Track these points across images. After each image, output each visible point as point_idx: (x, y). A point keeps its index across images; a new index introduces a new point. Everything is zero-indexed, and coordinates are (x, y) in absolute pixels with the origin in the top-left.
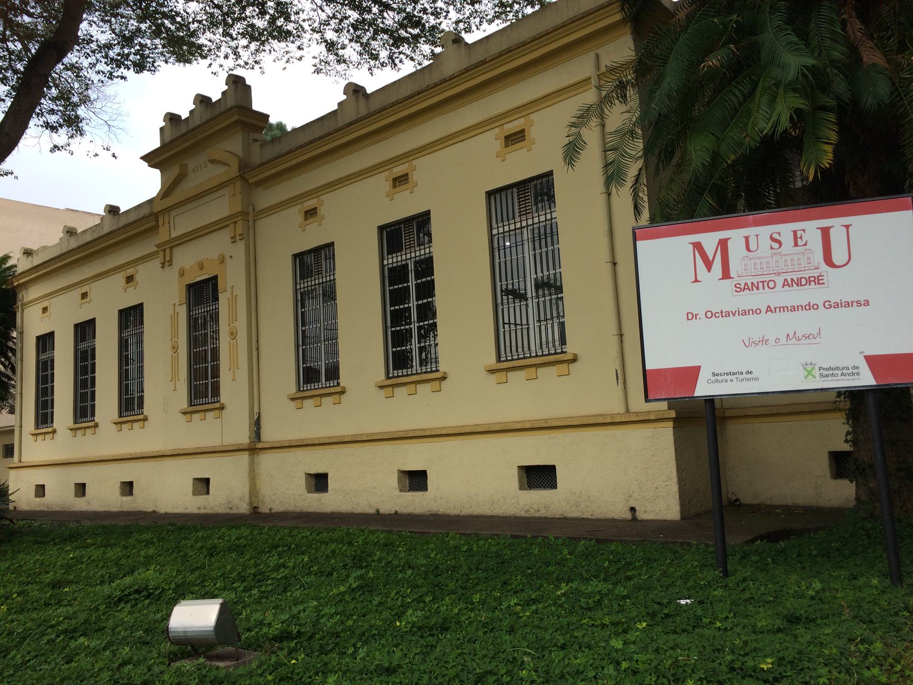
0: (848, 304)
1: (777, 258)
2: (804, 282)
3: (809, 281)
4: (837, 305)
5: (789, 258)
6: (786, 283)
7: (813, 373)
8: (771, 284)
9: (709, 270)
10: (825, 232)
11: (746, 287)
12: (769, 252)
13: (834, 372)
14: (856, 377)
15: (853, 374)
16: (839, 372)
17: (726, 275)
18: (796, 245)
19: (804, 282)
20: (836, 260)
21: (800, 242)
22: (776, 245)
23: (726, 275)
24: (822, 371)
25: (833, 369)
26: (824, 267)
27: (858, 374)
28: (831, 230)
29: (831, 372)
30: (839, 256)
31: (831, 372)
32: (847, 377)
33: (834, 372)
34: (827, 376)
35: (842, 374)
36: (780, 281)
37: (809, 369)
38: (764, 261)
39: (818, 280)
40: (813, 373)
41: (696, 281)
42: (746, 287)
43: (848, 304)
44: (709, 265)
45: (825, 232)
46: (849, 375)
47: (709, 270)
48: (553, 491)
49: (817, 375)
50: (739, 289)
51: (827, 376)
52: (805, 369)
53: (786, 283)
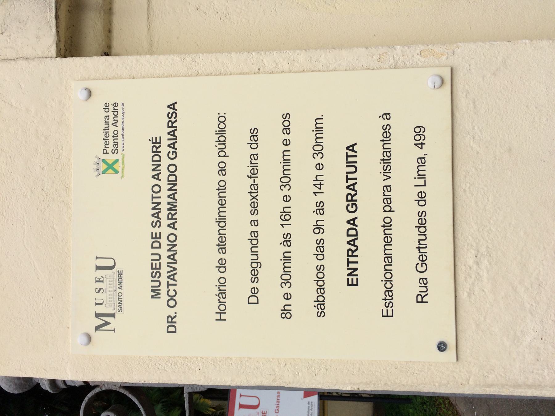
0: (278, 401)
1: (108, 291)
2: (120, 280)
3: (120, 277)
4: (278, 407)
5: (108, 285)
6: (120, 288)
7: (110, 162)
8: (120, 294)
9: (110, 323)
10: (241, 406)
11: (120, 306)
12: (104, 294)
13: (111, 134)
14: (119, 108)
15: (115, 111)
16: (112, 128)
17: (113, 315)
18: (102, 281)
19: (120, 280)
20: (112, 264)
21: (102, 280)
22: (102, 291)
23: (113, 315)
24: (109, 150)
25: (172, 217)
26: (114, 270)
27: (115, 105)
28: (241, 403)
29: (111, 140)
30: (110, 263)
31: (111, 140)
32: (119, 118)
33: (111, 134)
34: (116, 144)
35: (115, 124)
36: (119, 291)
37: (105, 167)
38: (108, 297)
39: (120, 273)
40: (110, 162)
41: (114, 330)
42: (120, 306)
43: (278, 401)
44: (107, 323)
45: (241, 406)
46: (116, 116)
47: (110, 323)
48: (53, 50)
49: (115, 156)
50: (120, 310)
51: (116, 144)
52: (104, 172)
53: (120, 288)
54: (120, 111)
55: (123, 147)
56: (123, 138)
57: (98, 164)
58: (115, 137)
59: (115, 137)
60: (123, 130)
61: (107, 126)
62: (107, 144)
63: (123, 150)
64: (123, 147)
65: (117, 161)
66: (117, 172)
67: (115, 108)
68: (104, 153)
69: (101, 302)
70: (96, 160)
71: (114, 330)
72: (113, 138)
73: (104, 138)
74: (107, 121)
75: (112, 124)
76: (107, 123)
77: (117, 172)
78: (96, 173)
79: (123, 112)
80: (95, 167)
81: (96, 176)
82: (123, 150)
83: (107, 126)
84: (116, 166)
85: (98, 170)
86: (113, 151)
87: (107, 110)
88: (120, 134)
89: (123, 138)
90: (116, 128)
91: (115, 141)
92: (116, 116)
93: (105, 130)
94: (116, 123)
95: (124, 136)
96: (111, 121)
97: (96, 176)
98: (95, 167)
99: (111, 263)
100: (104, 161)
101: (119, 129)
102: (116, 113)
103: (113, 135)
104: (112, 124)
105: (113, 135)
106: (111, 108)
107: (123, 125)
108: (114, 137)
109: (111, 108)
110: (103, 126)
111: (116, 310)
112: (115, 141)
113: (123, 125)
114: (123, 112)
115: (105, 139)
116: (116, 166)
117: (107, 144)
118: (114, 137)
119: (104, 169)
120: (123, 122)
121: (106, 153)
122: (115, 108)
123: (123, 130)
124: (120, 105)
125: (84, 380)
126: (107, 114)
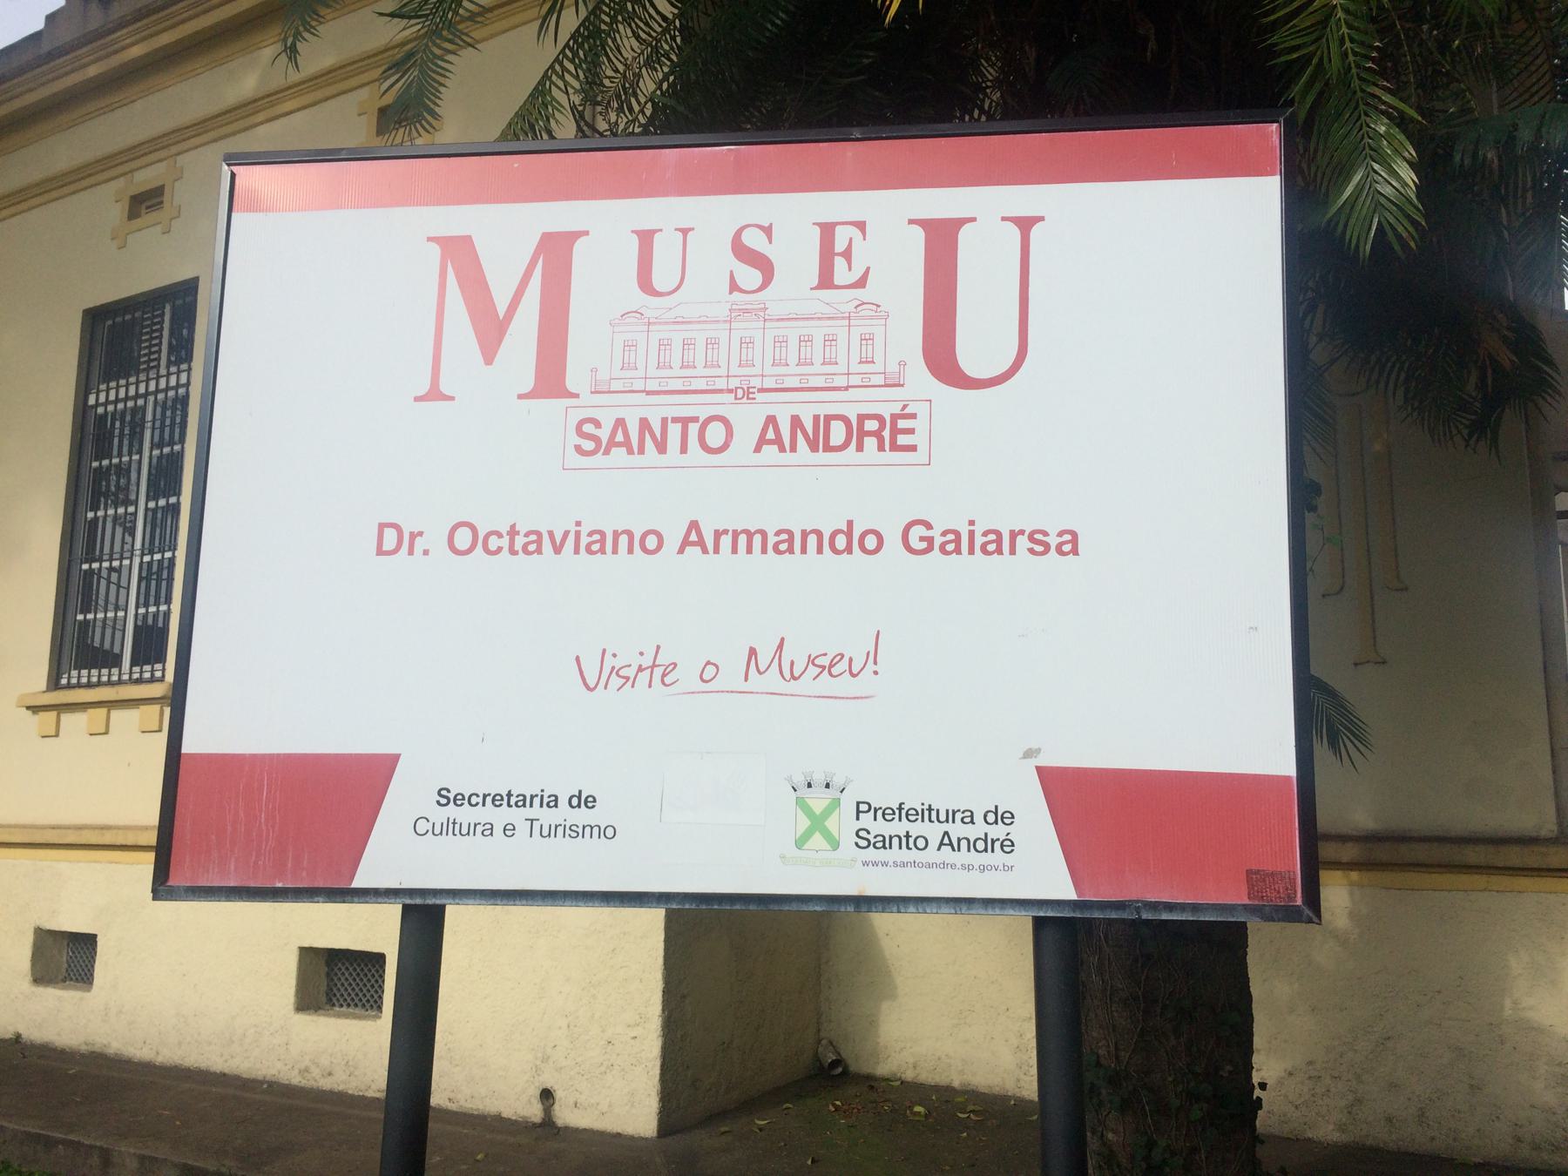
2: (838, 433)
3: (857, 433)
5: (793, 332)
8: (715, 435)
9: (489, 356)
13: (916, 829)
14: (998, 857)
15: (989, 844)
16: (934, 832)
17: (550, 380)
18: (826, 280)
19: (838, 433)
20: (970, 359)
21: (841, 273)
22: (750, 277)
23: (550, 380)
24: (866, 820)
26: (921, 381)
27: (1008, 845)
29: (899, 827)
31: (899, 827)
32: (964, 857)
33: (916, 829)
34: (885, 843)
36: (748, 420)
39: (891, 433)
41: (434, 394)
42: (620, 439)
44: (491, 332)
46: (972, 845)
47: (489, 356)
50: (595, 441)
51: (885, 843)
52: (801, 803)
54: (986, 858)
55: (875, 864)
56: (904, 865)
57: (827, 786)
58: (907, 840)
59: (907, 840)
60: (929, 866)
61: (943, 818)
62: (886, 814)
63: (865, 864)
64: (875, 864)
65: (835, 845)
66: (800, 843)
67: (997, 845)
68: (858, 804)
69: (663, 276)
70: (838, 781)
71: (434, 394)
72: (902, 834)
73: (906, 807)
74: (959, 816)
75: (946, 833)
76: (951, 816)
77: (800, 843)
78: (800, 780)
79: (983, 869)
80: (818, 778)
81: (790, 779)
82: (865, 864)
83: (943, 818)
84: (817, 840)
85: (809, 785)
86: (862, 834)
87: (991, 818)
88: (914, 855)
89: (904, 865)
90: (934, 843)
91: (895, 841)
92: (972, 845)
93: (930, 809)
94: (951, 844)
95: (908, 870)
96: (957, 830)
97: (790, 779)
98: (818, 778)
99: (979, 347)
100: (836, 803)
101: (931, 855)
102: (980, 845)
103: (914, 834)
104: (946, 833)
105: (914, 834)
106: (998, 832)
107: (944, 865)
108: (908, 836)
109: (998, 832)
110: (942, 805)
111: (589, 403)
112: (895, 841)
113: (944, 865)
114: (983, 869)
115: (900, 809)
116: (817, 840)
117: (886, 814)
118: (908, 836)
119: (811, 803)
120: (953, 866)
121: (858, 812)
122: (997, 845)
123: (929, 866)
124: (1008, 859)
125: (306, 945)
126: (978, 818)
